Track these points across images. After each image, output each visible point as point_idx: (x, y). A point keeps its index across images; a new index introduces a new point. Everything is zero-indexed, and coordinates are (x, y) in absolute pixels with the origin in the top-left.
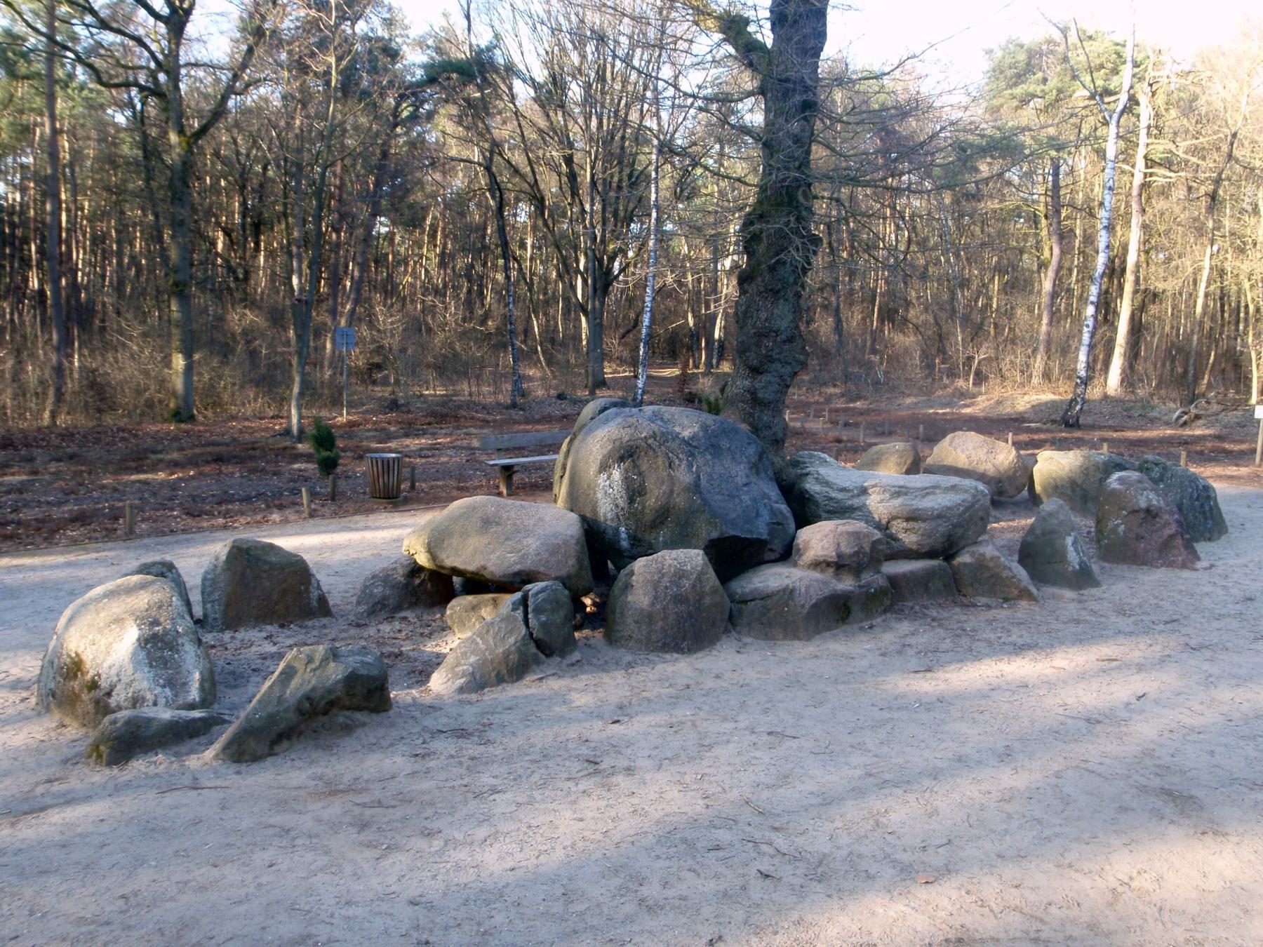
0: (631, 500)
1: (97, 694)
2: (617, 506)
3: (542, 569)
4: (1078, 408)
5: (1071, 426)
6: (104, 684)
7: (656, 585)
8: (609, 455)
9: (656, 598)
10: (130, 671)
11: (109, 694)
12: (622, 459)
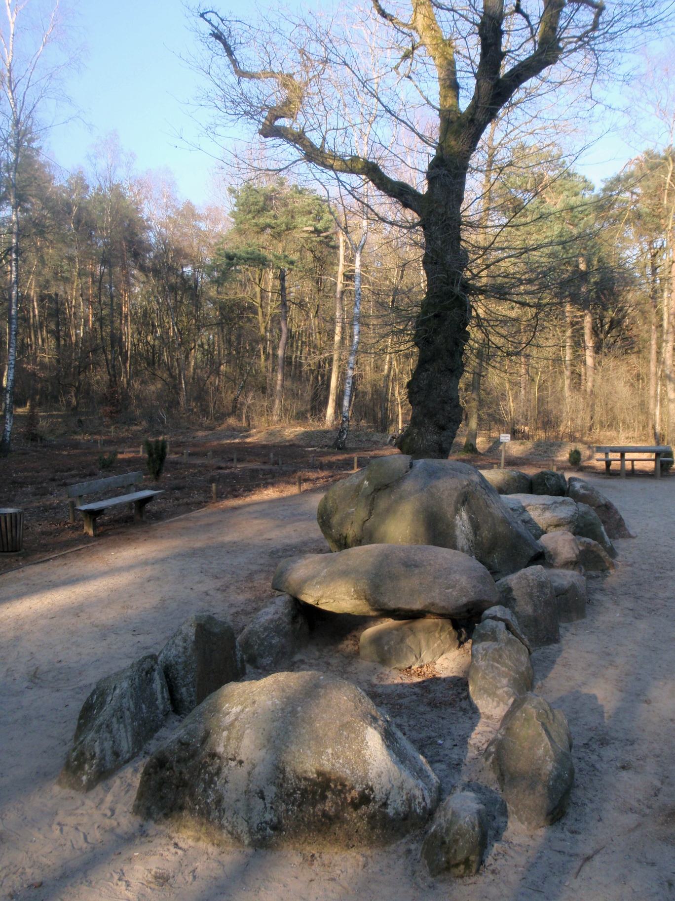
0: (475, 534)
1: (372, 807)
2: (468, 540)
3: (486, 598)
4: (345, 437)
5: (341, 449)
6: (378, 795)
7: (531, 595)
8: (457, 502)
9: (535, 605)
10: (397, 774)
11: (385, 805)
12: (463, 504)
